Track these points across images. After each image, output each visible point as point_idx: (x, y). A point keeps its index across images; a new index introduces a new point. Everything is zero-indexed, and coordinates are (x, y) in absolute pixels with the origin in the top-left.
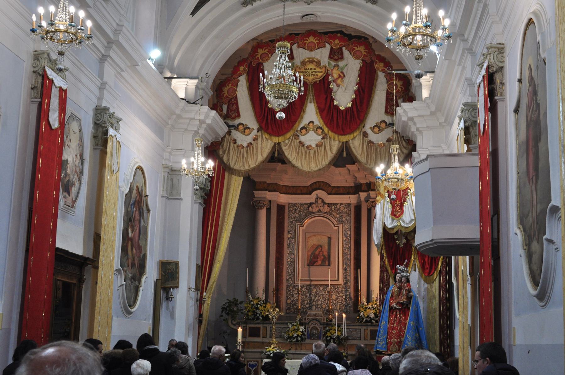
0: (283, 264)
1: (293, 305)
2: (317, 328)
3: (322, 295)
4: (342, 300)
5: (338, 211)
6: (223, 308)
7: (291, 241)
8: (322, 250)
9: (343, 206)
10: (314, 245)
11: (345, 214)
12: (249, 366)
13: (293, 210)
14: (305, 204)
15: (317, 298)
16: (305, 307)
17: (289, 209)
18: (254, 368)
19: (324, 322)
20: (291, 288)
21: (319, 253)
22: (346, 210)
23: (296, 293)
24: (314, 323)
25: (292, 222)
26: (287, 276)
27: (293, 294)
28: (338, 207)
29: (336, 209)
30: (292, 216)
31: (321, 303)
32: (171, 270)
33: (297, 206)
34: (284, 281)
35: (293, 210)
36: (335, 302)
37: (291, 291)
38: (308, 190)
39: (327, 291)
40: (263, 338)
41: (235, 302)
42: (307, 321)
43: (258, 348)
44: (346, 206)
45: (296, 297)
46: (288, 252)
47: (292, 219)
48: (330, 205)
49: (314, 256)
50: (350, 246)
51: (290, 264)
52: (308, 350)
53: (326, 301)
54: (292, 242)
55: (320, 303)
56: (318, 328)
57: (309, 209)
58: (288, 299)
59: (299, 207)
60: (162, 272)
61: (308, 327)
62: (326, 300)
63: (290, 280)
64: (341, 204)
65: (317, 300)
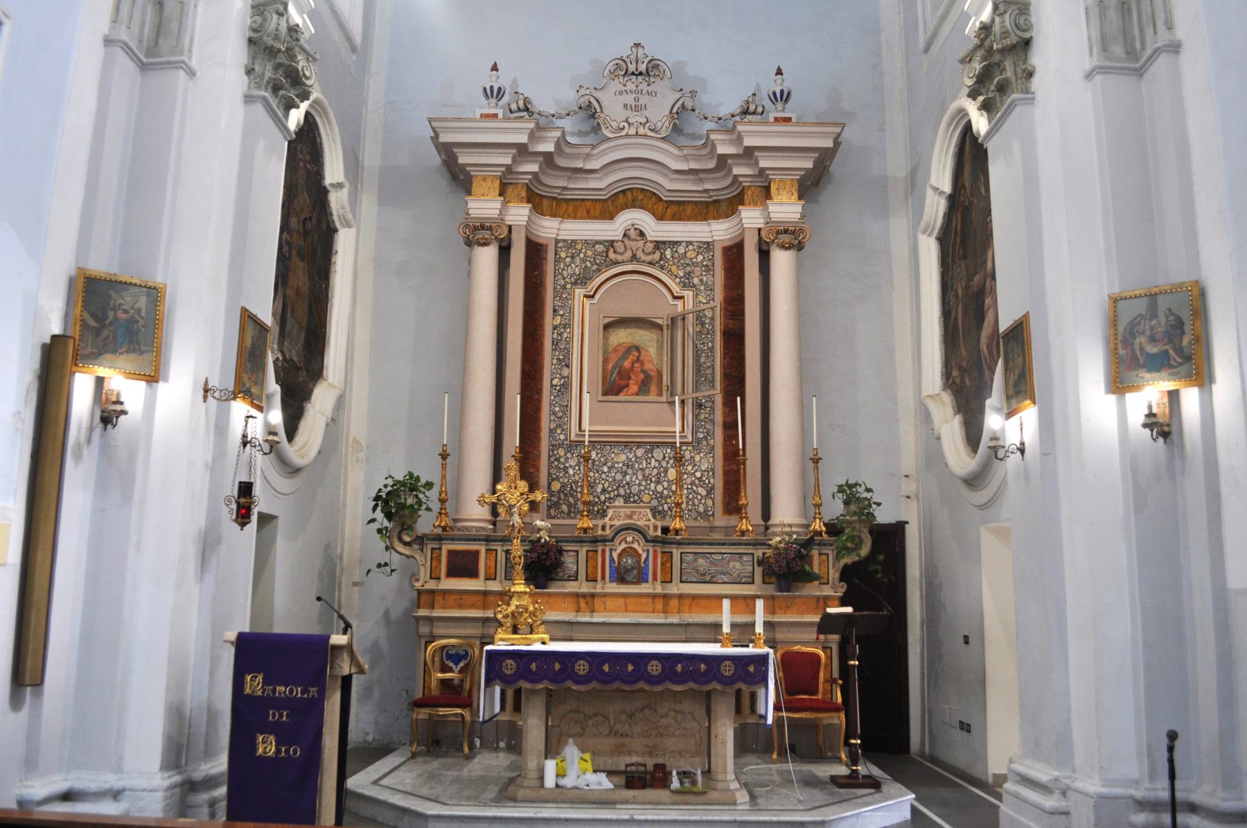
0: (539, 392)
1: (565, 495)
2: (637, 551)
3: (642, 470)
4: (693, 483)
5: (682, 261)
6: (377, 498)
7: (561, 334)
8: (641, 358)
9: (694, 250)
10: (619, 345)
11: (698, 269)
12: (447, 660)
13: (566, 257)
14: (598, 242)
15: (628, 478)
16: (596, 500)
17: (556, 254)
18: (462, 664)
19: (657, 536)
20: (561, 452)
21: (633, 366)
22: (700, 258)
23: (573, 463)
24: (629, 539)
25: (564, 287)
26: (550, 421)
27: (565, 469)
28: (681, 250)
29: (676, 255)
30: (565, 273)
31: (640, 491)
32: (125, 311)
33: (579, 247)
34: (544, 434)
35: (566, 257)
36: (674, 488)
37: (562, 460)
38: (606, 208)
39: (653, 460)
40: (486, 579)
41: (411, 484)
42: (608, 532)
43: (473, 606)
44: (700, 248)
45: (574, 475)
46: (555, 362)
47: (564, 279)
48: (659, 245)
49: (619, 372)
50: (713, 347)
51: (559, 391)
52: (612, 611)
53: (653, 486)
54: (565, 335)
55: (635, 489)
56: (640, 552)
57: (607, 256)
58: (553, 480)
59: (583, 251)
60: (86, 316)
61: (611, 550)
62: (651, 482)
63: (559, 431)
64: (691, 243)
65: (628, 483)
